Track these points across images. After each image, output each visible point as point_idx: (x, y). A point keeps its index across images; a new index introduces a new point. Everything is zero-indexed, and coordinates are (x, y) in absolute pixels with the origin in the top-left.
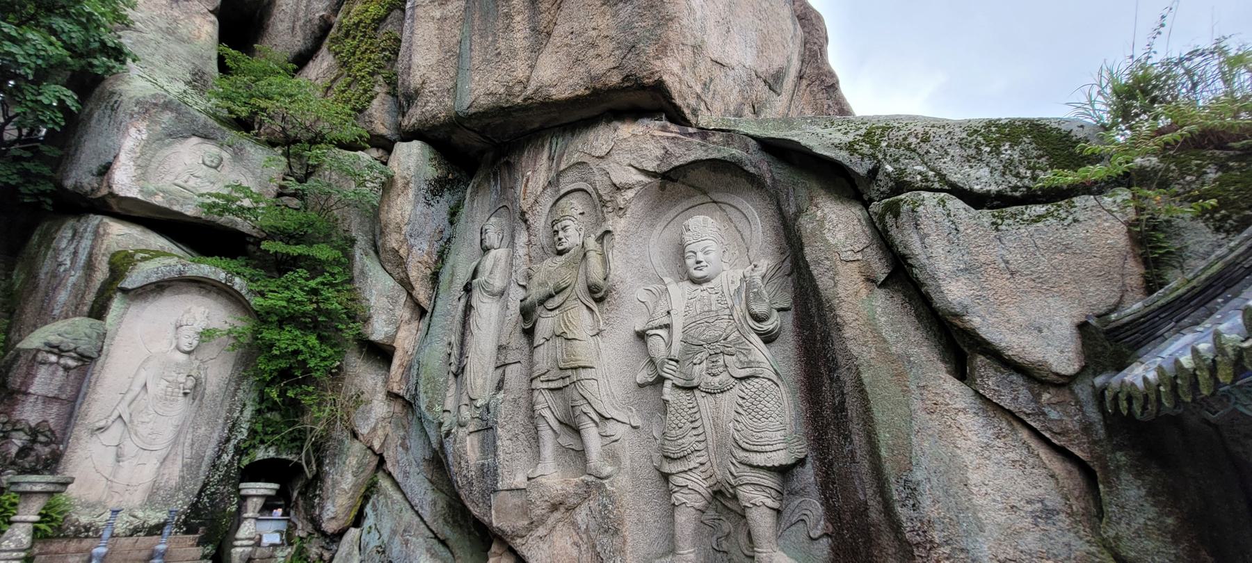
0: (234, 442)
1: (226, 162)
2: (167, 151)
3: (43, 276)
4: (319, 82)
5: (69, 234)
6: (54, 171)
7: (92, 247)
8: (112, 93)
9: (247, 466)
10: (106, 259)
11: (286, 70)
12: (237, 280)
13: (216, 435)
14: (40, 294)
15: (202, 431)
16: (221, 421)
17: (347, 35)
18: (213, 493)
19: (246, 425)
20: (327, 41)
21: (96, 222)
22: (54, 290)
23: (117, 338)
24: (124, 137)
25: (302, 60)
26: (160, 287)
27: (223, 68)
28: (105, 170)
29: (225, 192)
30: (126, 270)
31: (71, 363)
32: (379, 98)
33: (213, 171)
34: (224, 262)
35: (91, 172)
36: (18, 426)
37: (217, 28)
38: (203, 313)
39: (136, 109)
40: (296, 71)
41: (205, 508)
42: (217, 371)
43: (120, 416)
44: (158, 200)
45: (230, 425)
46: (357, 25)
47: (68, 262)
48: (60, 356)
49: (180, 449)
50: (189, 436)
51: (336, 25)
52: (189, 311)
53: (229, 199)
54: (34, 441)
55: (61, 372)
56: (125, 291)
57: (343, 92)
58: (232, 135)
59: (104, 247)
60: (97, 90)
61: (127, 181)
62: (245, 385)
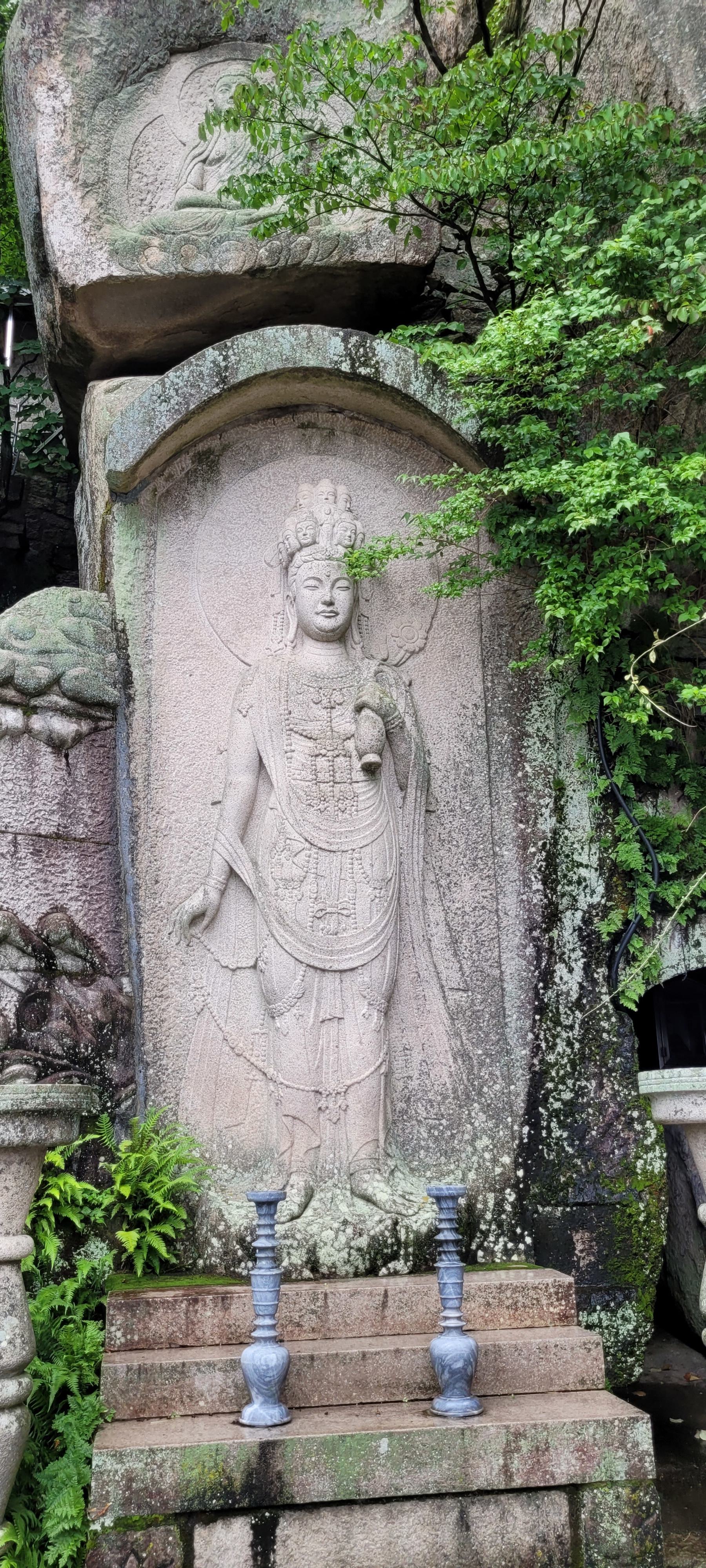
0: (571, 920)
2: (132, 125)
9: (643, 1002)
13: (510, 903)
16: (509, 853)
18: (571, 1107)
19: (589, 856)
23: (157, 640)
24: (32, 122)
31: (64, 727)
41: (565, 1162)
43: (232, 874)
44: (155, 262)
48: (29, 710)
49: (423, 961)
50: (436, 914)
54: (49, 970)
55: (47, 759)
62: (538, 721)
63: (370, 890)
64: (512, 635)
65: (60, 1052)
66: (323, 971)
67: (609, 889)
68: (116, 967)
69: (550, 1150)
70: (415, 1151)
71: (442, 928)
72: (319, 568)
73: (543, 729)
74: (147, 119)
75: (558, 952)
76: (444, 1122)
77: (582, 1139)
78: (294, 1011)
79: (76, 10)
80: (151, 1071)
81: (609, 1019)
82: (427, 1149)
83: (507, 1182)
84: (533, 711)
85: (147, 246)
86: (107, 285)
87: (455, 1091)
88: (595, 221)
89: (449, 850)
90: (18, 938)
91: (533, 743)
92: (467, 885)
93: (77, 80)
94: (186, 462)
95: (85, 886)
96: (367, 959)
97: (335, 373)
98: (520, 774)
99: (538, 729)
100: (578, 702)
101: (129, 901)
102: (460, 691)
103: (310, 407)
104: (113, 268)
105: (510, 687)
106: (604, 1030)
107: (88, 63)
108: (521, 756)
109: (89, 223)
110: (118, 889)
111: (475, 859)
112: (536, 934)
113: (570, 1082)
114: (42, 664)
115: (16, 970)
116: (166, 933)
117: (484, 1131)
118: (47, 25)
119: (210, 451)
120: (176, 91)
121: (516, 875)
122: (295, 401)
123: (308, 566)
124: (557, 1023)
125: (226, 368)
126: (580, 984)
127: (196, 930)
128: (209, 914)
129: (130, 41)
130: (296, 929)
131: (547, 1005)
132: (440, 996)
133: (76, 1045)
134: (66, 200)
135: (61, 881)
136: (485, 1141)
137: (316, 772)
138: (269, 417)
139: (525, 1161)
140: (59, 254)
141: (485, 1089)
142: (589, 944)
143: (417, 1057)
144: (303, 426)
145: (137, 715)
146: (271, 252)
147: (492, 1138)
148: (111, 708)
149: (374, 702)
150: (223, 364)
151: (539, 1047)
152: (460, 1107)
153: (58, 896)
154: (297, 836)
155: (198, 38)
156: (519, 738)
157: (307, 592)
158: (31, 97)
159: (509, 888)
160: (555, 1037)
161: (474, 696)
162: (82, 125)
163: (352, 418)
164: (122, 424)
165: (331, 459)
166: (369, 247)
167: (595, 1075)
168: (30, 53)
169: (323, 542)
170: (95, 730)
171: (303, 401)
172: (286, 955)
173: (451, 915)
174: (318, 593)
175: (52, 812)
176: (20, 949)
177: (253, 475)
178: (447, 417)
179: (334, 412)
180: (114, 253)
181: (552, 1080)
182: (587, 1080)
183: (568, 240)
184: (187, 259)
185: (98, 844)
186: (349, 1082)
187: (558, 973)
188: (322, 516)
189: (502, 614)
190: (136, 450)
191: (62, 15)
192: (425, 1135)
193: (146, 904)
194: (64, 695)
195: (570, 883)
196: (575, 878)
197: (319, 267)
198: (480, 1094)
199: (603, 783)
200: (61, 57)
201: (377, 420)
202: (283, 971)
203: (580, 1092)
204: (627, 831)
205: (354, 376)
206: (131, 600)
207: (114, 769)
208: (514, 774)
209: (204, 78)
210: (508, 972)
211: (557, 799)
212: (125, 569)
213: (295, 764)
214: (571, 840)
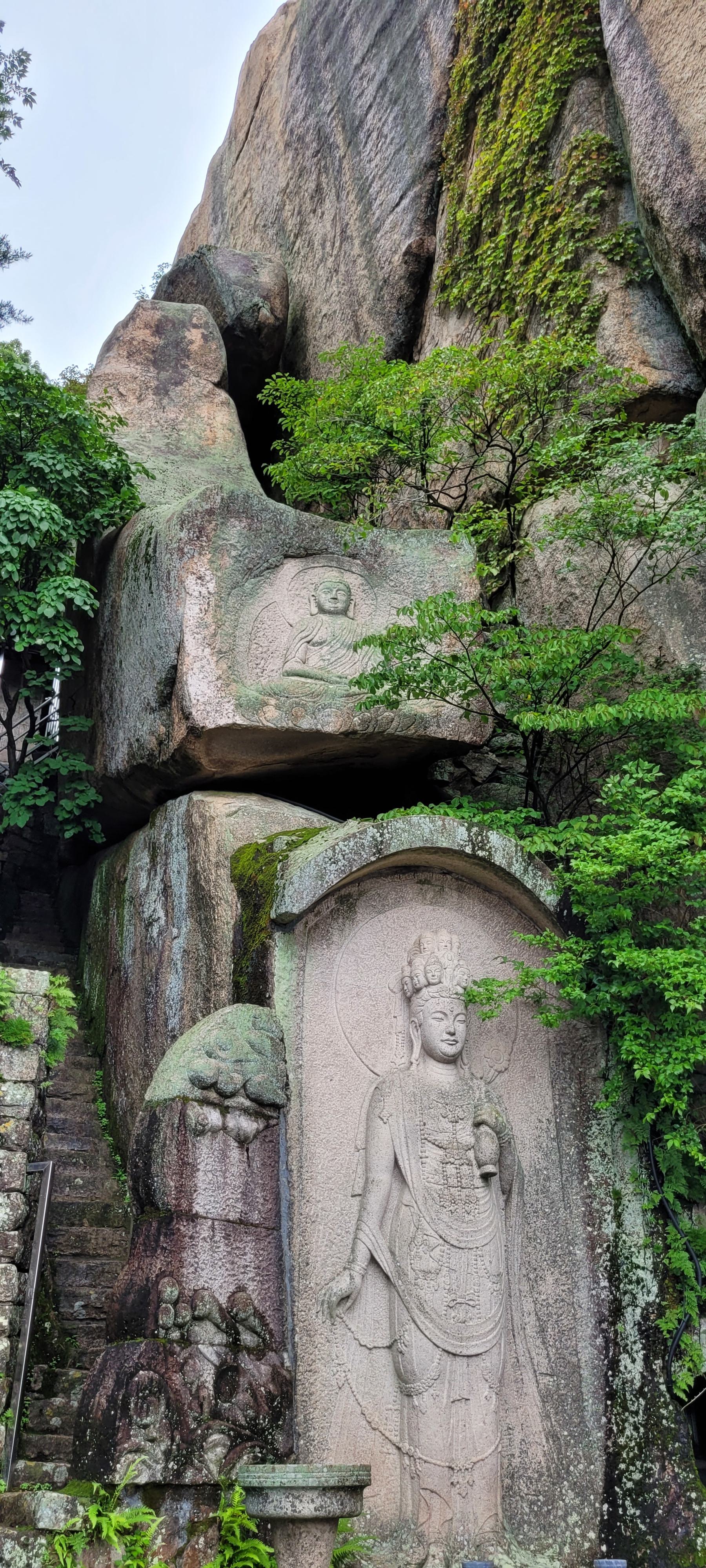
0: (633, 1315)
1: (358, 595)
2: (254, 609)
3: (128, 961)
5: (145, 859)
6: (90, 761)
7: (193, 861)
10: (224, 873)
13: (583, 1296)
14: (136, 999)
15: (549, 1287)
16: (580, 1252)
17: (475, 241)
18: (641, 1487)
21: (183, 809)
22: (156, 978)
23: (306, 1048)
26: (344, 899)
28: (170, 687)
30: (274, 876)
32: (612, 307)
33: (341, 620)
36: (201, 1311)
37: (234, 410)
38: (448, 948)
43: (373, 1260)
44: (272, 717)
47: (161, 913)
50: (529, 1306)
55: (235, 1153)
56: (286, 924)
59: (213, 848)
61: (210, 692)
63: (490, 1284)
64: (573, 1063)
65: (243, 1423)
66: (454, 1355)
67: (661, 1289)
68: (280, 1343)
69: (627, 1526)
70: (520, 1525)
71: (533, 1317)
72: (445, 1004)
73: (602, 1145)
74: (264, 604)
75: (622, 1343)
76: (541, 1498)
77: (652, 1517)
78: (431, 1391)
79: (222, 523)
80: (302, 1442)
81: (667, 1407)
82: (529, 1523)
84: (593, 1129)
85: (266, 704)
86: (230, 730)
87: (549, 1470)
88: (661, 774)
89: (535, 1247)
90: (217, 1316)
91: (595, 1156)
92: (550, 1279)
93: (219, 574)
95: (259, 1268)
96: (489, 1345)
97: (460, 854)
98: (586, 1183)
99: (598, 1145)
101: (287, 1281)
102: (536, 1106)
104: (237, 718)
105: (574, 1107)
106: (663, 1417)
107: (228, 561)
108: (586, 1167)
109: (221, 681)
110: (279, 1270)
111: (555, 1256)
112: (604, 1326)
113: (638, 1464)
114: (236, 1071)
115: (212, 1345)
116: (314, 1312)
117: (574, 1508)
118: (200, 532)
119: (350, 895)
120: (286, 585)
121: (586, 1272)
122: (418, 864)
124: (625, 1409)
125: (382, 842)
126: (641, 1373)
127: (340, 1311)
128: (353, 1296)
129: (258, 547)
130: (434, 1316)
131: (616, 1391)
132: (534, 1381)
133: (257, 1417)
134: (204, 661)
135: (243, 1263)
136: (574, 1518)
137: (446, 1178)
138: (396, 873)
139: (607, 1537)
140: (194, 702)
141: (572, 1468)
142: (647, 1337)
144: (420, 882)
145: (291, 1113)
146: (363, 721)
147: (580, 1514)
148: (276, 1107)
149: (491, 1121)
150: (379, 839)
151: (611, 1430)
152: (554, 1484)
153: (241, 1276)
154: (433, 1233)
155: (306, 549)
157: (434, 1023)
158: (182, 582)
159: (582, 1284)
160: (624, 1421)
161: (547, 1112)
162: (220, 607)
163: (457, 879)
164: (300, 877)
165: (441, 909)
166: (438, 726)
167: (658, 1458)
168: (186, 550)
169: (446, 983)
170: (267, 1127)
171: (424, 864)
172: (426, 1340)
173: (539, 1306)
174: (443, 1024)
175: (237, 1200)
176: (217, 1326)
177: (381, 917)
178: (537, 892)
179: (444, 874)
180: (239, 706)
181: (624, 1462)
182: (652, 1462)
183: (641, 783)
184: (297, 717)
185: (267, 1229)
186: (475, 1459)
187: (623, 1363)
189: (564, 1044)
190: (309, 898)
191: (212, 526)
192: (527, 1510)
193: (299, 1285)
194: (248, 1097)
195: (630, 1282)
196: (634, 1278)
197: (398, 736)
198: (568, 1472)
199: (657, 1198)
200: (209, 556)
201: (475, 882)
202: (421, 1354)
203: (647, 1473)
204: (675, 1240)
205: (474, 856)
206: (287, 1013)
207: (278, 1162)
208: (581, 1183)
209: (307, 577)
210: (583, 1360)
211: (616, 1207)
212: (283, 987)
213: (428, 1169)
214: (629, 1244)
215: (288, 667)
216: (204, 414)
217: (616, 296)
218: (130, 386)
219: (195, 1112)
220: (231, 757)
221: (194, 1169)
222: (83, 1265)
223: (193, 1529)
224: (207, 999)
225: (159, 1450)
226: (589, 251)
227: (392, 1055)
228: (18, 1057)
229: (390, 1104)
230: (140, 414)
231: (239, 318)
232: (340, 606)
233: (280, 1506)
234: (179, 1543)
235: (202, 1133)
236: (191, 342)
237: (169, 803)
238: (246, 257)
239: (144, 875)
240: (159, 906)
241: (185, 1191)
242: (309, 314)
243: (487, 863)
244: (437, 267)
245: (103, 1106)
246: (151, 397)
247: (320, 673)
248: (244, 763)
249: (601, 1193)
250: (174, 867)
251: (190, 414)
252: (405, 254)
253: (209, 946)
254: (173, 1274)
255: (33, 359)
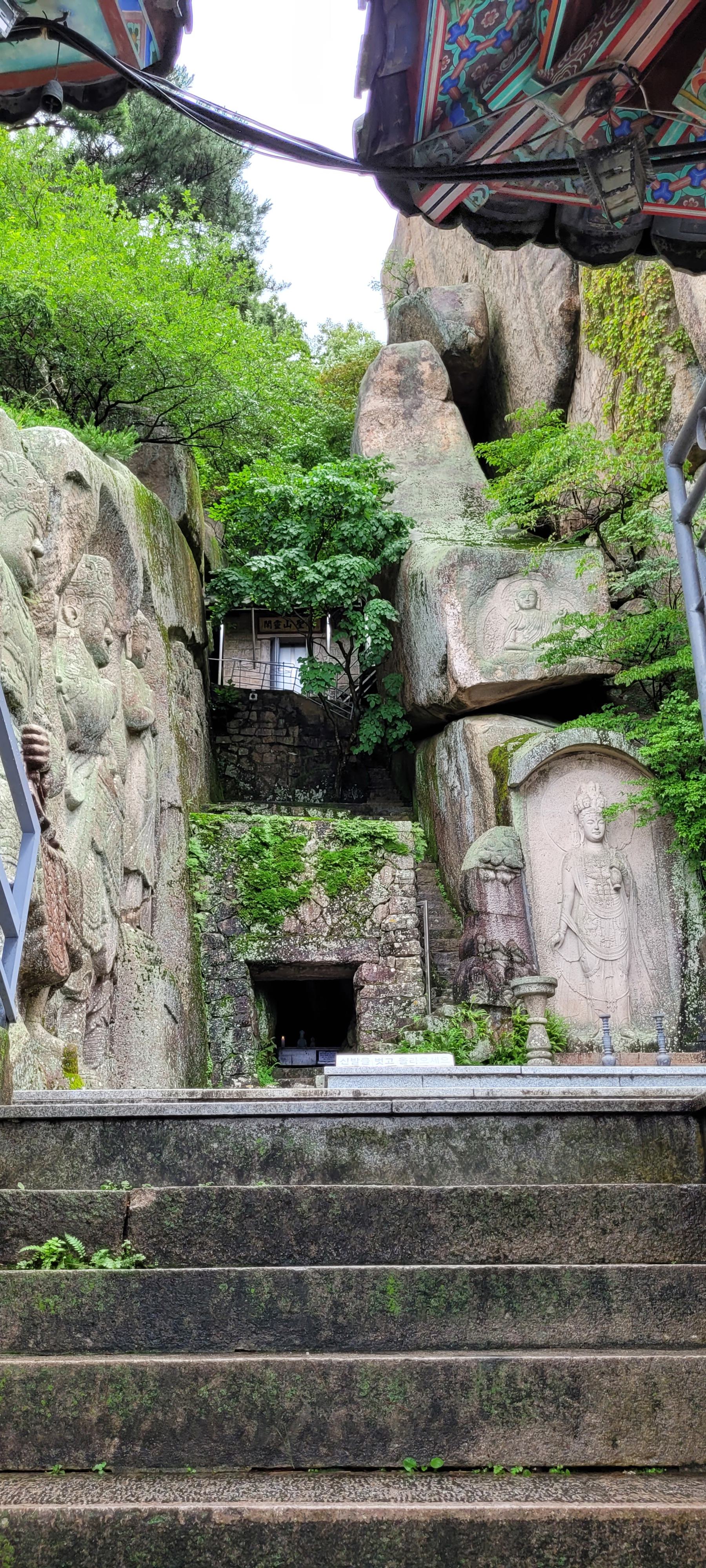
2: (484, 615)
4: (597, 408)
7: (470, 757)
8: (414, 576)
10: (486, 763)
11: (553, 424)
12: (611, 734)
13: (670, 938)
14: (451, 828)
16: (668, 920)
17: (602, 314)
20: (583, 338)
21: (461, 728)
23: (531, 843)
24: (444, 620)
25: (563, 394)
26: (542, 773)
27: (490, 472)
28: (445, 666)
29: (556, 630)
32: (679, 383)
33: (533, 612)
34: (591, 719)
35: (434, 674)
36: (495, 947)
38: (591, 790)
39: (440, 581)
40: (564, 418)
42: (641, 855)
43: (568, 927)
44: (500, 676)
45: (680, 922)
46: (607, 290)
47: (458, 783)
49: (639, 959)
50: (642, 942)
51: (583, 308)
52: (580, 792)
53: (563, 638)
55: (502, 888)
56: (515, 788)
57: (632, 404)
58: (537, 554)
59: (479, 750)
60: (400, 580)
62: (677, 870)
83: (674, 1035)
86: (480, 685)
91: (676, 878)
92: (653, 932)
94: (536, 775)
97: (595, 744)
100: (692, 863)
103: (582, 752)
107: (466, 591)
110: (528, 933)
123: (587, 816)
143: (639, 993)
156: (670, 876)
169: (593, 806)
174: (593, 826)
180: (482, 673)
183: (679, 701)
188: (592, 797)
202: (591, 961)
205: (602, 745)
215: (506, 645)
216: (439, 426)
217: (681, 375)
218: (387, 416)
219: (482, 873)
220: (482, 698)
221: (486, 895)
222: (445, 954)
223: (502, 1021)
224: (485, 826)
225: (486, 993)
226: (663, 345)
227: (573, 841)
228: (404, 859)
229: (570, 863)
230: (396, 436)
231: (454, 344)
232: (531, 604)
233: (524, 990)
234: (497, 1025)
235: (487, 881)
236: (423, 373)
237: (453, 723)
238: (453, 293)
239: (445, 762)
240: (456, 780)
241: (483, 904)
242: (505, 322)
243: (609, 747)
244: (583, 317)
245: (442, 887)
246: (402, 421)
247: (523, 646)
248: (490, 700)
249: (678, 894)
250: (461, 759)
251: (430, 428)
252: (560, 309)
253: (483, 800)
254: (483, 935)
255: (289, 309)
